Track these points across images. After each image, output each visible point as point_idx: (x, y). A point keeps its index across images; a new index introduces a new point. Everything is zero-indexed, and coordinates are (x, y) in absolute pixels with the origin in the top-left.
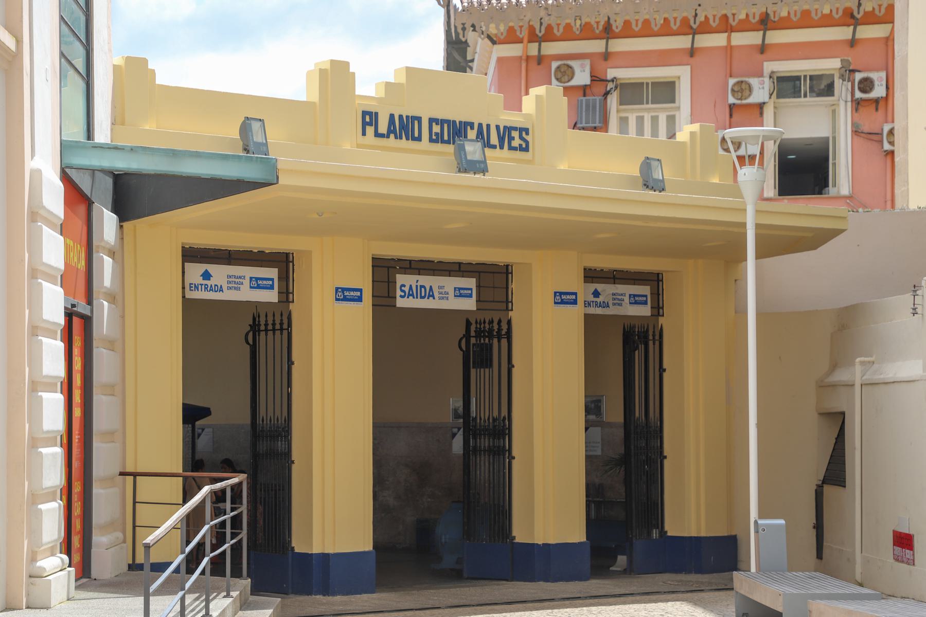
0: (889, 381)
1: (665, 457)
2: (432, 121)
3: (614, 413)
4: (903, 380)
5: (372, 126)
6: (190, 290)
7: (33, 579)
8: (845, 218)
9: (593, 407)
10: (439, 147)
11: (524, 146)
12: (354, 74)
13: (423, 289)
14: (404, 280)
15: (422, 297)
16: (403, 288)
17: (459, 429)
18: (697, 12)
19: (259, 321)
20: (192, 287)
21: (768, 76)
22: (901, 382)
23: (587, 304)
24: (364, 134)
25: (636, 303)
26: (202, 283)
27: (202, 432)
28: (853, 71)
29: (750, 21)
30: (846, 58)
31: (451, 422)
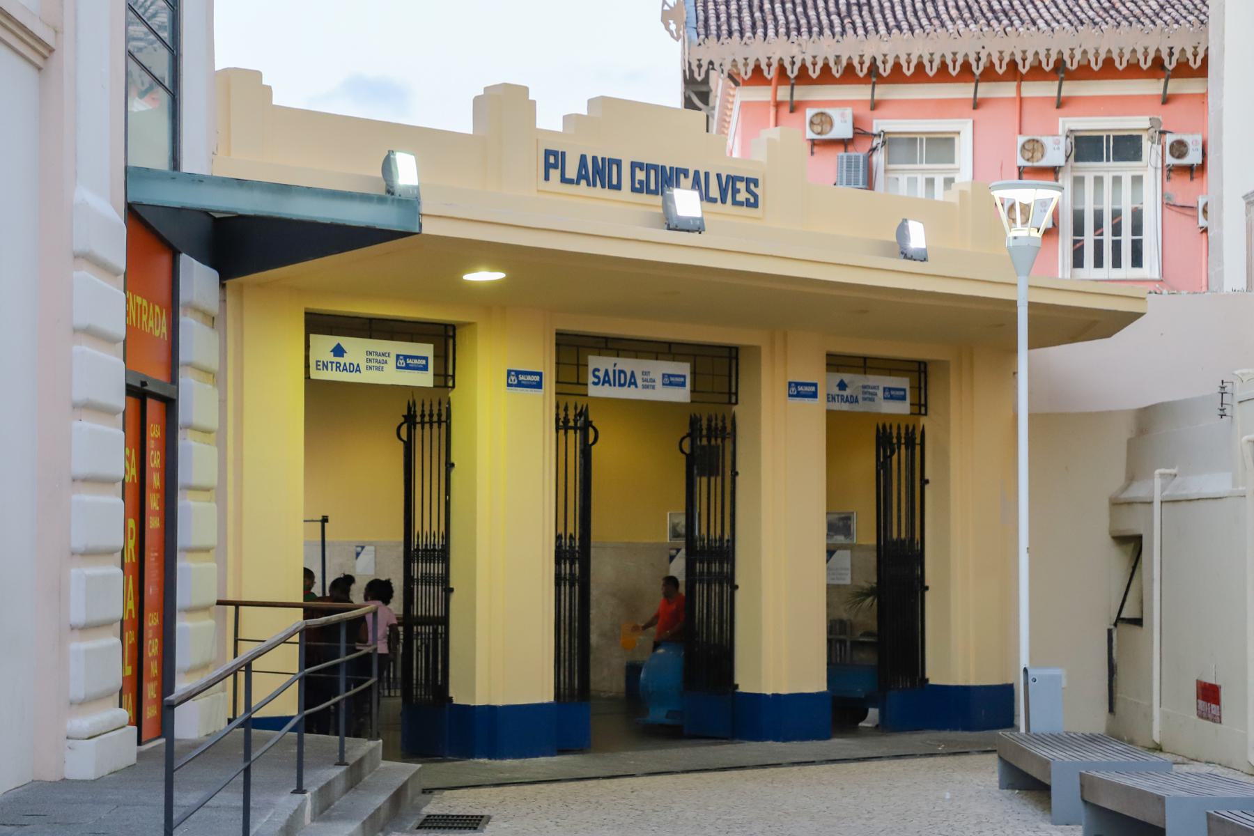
0: (1193, 498)
1: (927, 588)
2: (634, 165)
3: (865, 533)
4: (1208, 497)
5: (558, 168)
6: (317, 369)
7: (71, 741)
8: (1144, 299)
9: (839, 525)
10: (644, 198)
11: (752, 200)
12: (534, 102)
13: (622, 375)
14: (599, 363)
15: (620, 385)
16: (597, 373)
17: (678, 550)
18: (980, 55)
19: (415, 411)
20: (319, 365)
21: (1065, 135)
22: (1207, 499)
23: (831, 398)
24: (547, 178)
25: (892, 398)
26: (332, 361)
27: (362, 550)
28: (1163, 133)
29: (1043, 69)
30: (1156, 117)
31: (668, 541)
